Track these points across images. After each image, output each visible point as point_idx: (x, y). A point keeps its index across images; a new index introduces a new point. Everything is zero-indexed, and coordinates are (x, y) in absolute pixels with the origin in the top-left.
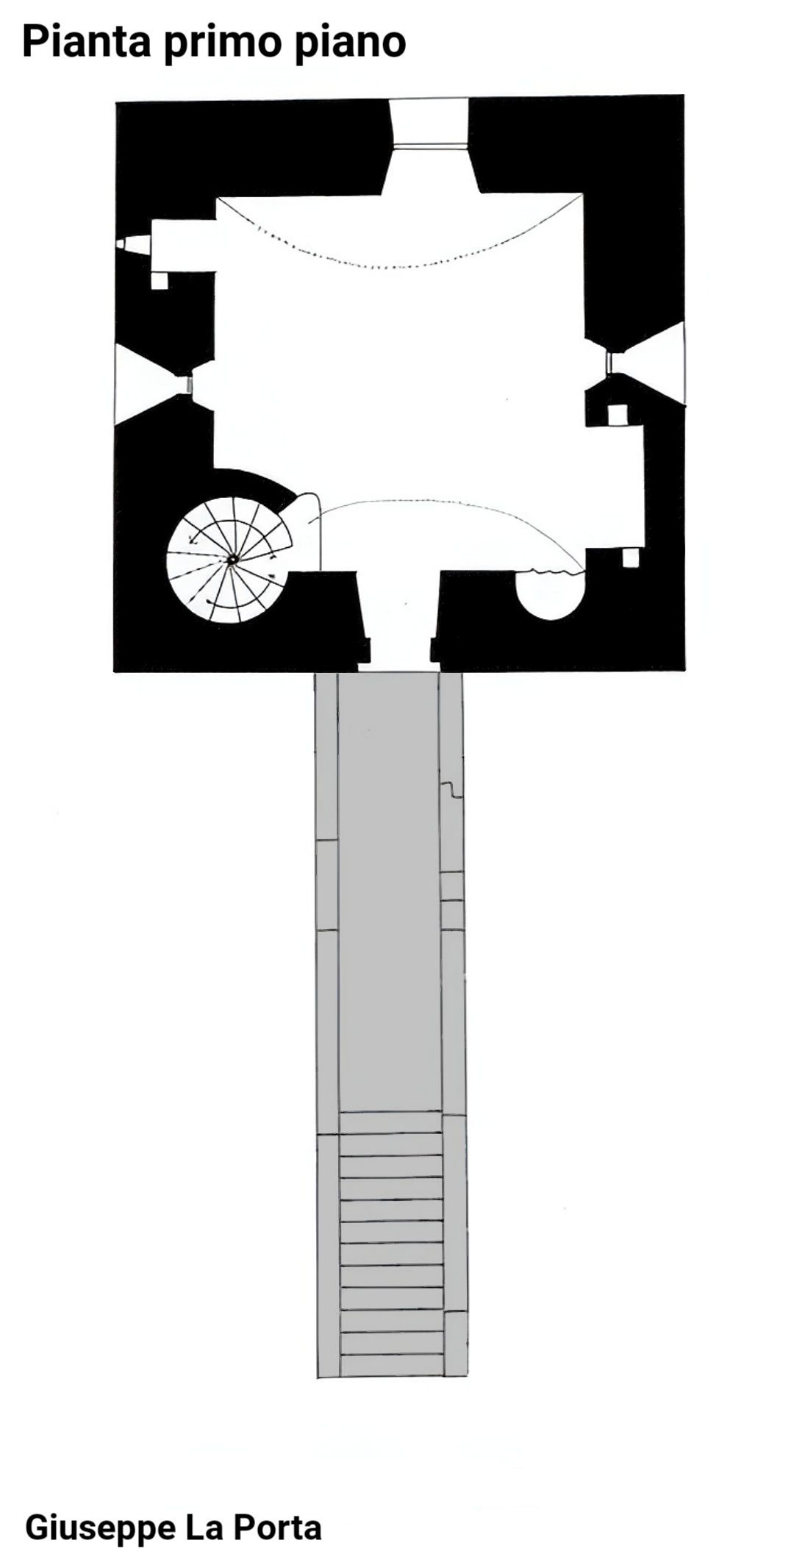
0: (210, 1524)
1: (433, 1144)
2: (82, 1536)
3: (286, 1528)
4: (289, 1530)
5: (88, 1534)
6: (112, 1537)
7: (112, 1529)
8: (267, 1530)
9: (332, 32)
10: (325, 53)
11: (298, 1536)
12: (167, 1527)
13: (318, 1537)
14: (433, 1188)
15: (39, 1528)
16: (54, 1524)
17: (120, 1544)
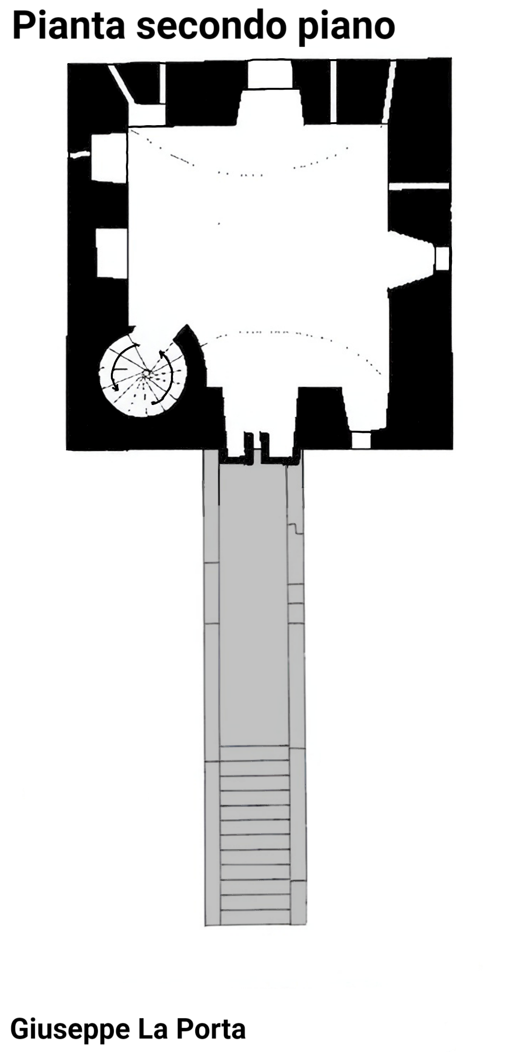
0: (157, 1026)
1: (283, 768)
2: (56, 1036)
3: (218, 1029)
4: (220, 1031)
5: (60, 1034)
6: (80, 1036)
7: (80, 1030)
8: (202, 1031)
9: (330, 18)
10: (325, 36)
11: (227, 1036)
12: (123, 1028)
13: (243, 1036)
14: (283, 797)
15: (21, 1029)
16: (33, 1026)
17: (86, 1042)
